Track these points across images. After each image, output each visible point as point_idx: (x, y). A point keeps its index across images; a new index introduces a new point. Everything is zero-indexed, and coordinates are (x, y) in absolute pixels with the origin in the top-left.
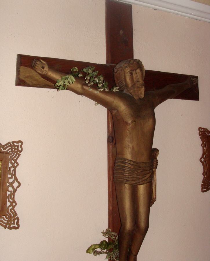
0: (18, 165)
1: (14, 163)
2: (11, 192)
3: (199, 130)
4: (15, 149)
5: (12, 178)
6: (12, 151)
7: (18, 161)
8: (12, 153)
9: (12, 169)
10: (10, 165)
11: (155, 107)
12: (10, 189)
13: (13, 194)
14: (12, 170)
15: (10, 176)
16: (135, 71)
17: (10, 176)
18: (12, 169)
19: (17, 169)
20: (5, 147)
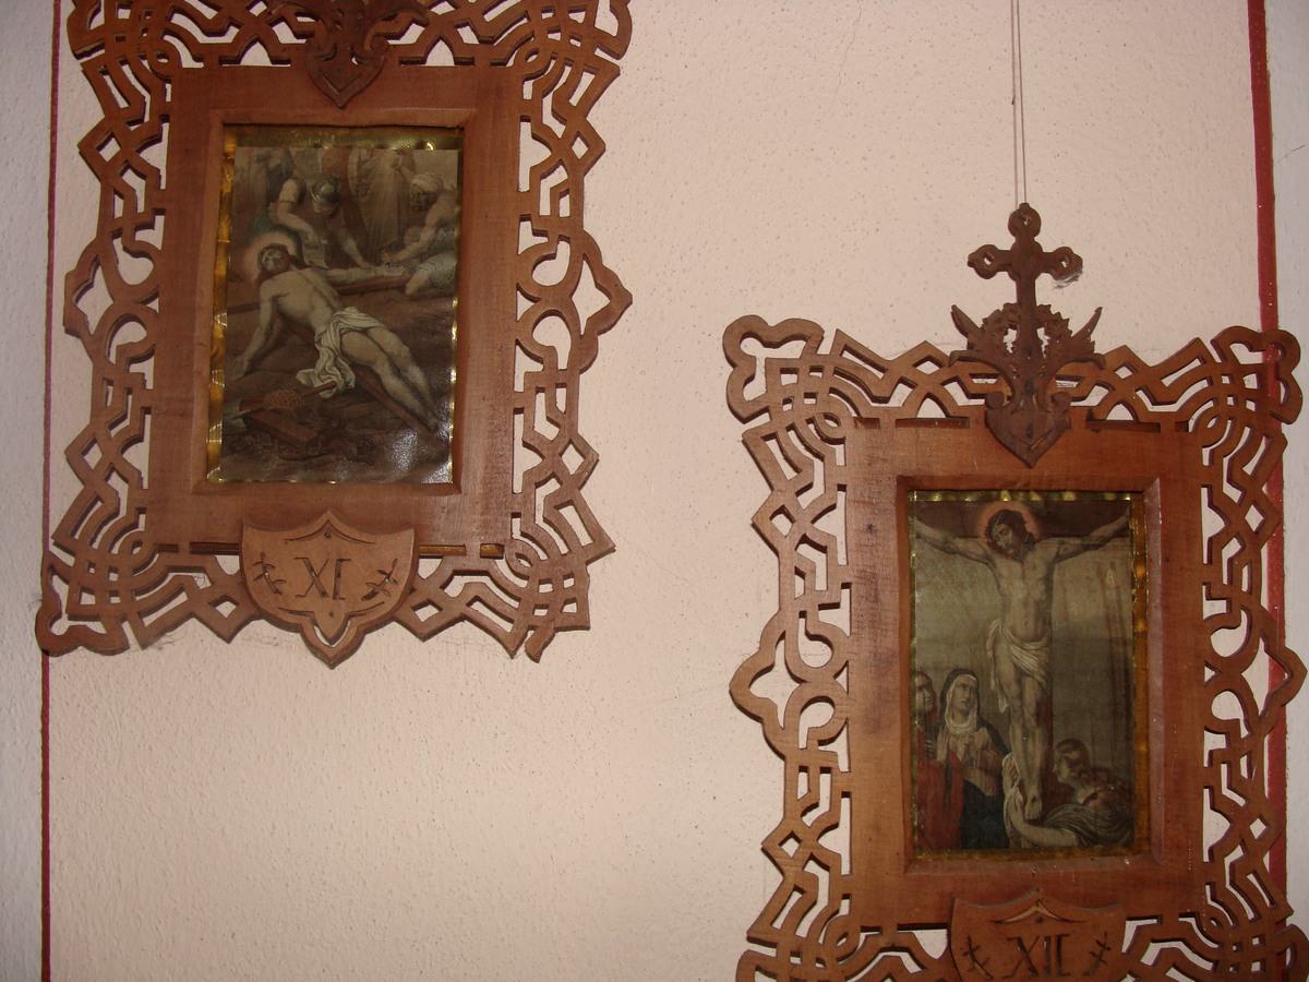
0: (597, 147)
1: (569, 139)
2: (1228, 729)
3: (733, 357)
4: (1243, 394)
5: (1227, 621)
6: (1220, 414)
7: (597, 117)
8: (1221, 426)
9: (1232, 548)
10: (1212, 523)
11: (572, 343)
12: (1226, 706)
13: (561, 378)
14: (1230, 561)
15: (1220, 607)
16: (1098, 774)
17: (1220, 607)
18: (1232, 548)
19: (592, 182)
20: (1167, 381)
